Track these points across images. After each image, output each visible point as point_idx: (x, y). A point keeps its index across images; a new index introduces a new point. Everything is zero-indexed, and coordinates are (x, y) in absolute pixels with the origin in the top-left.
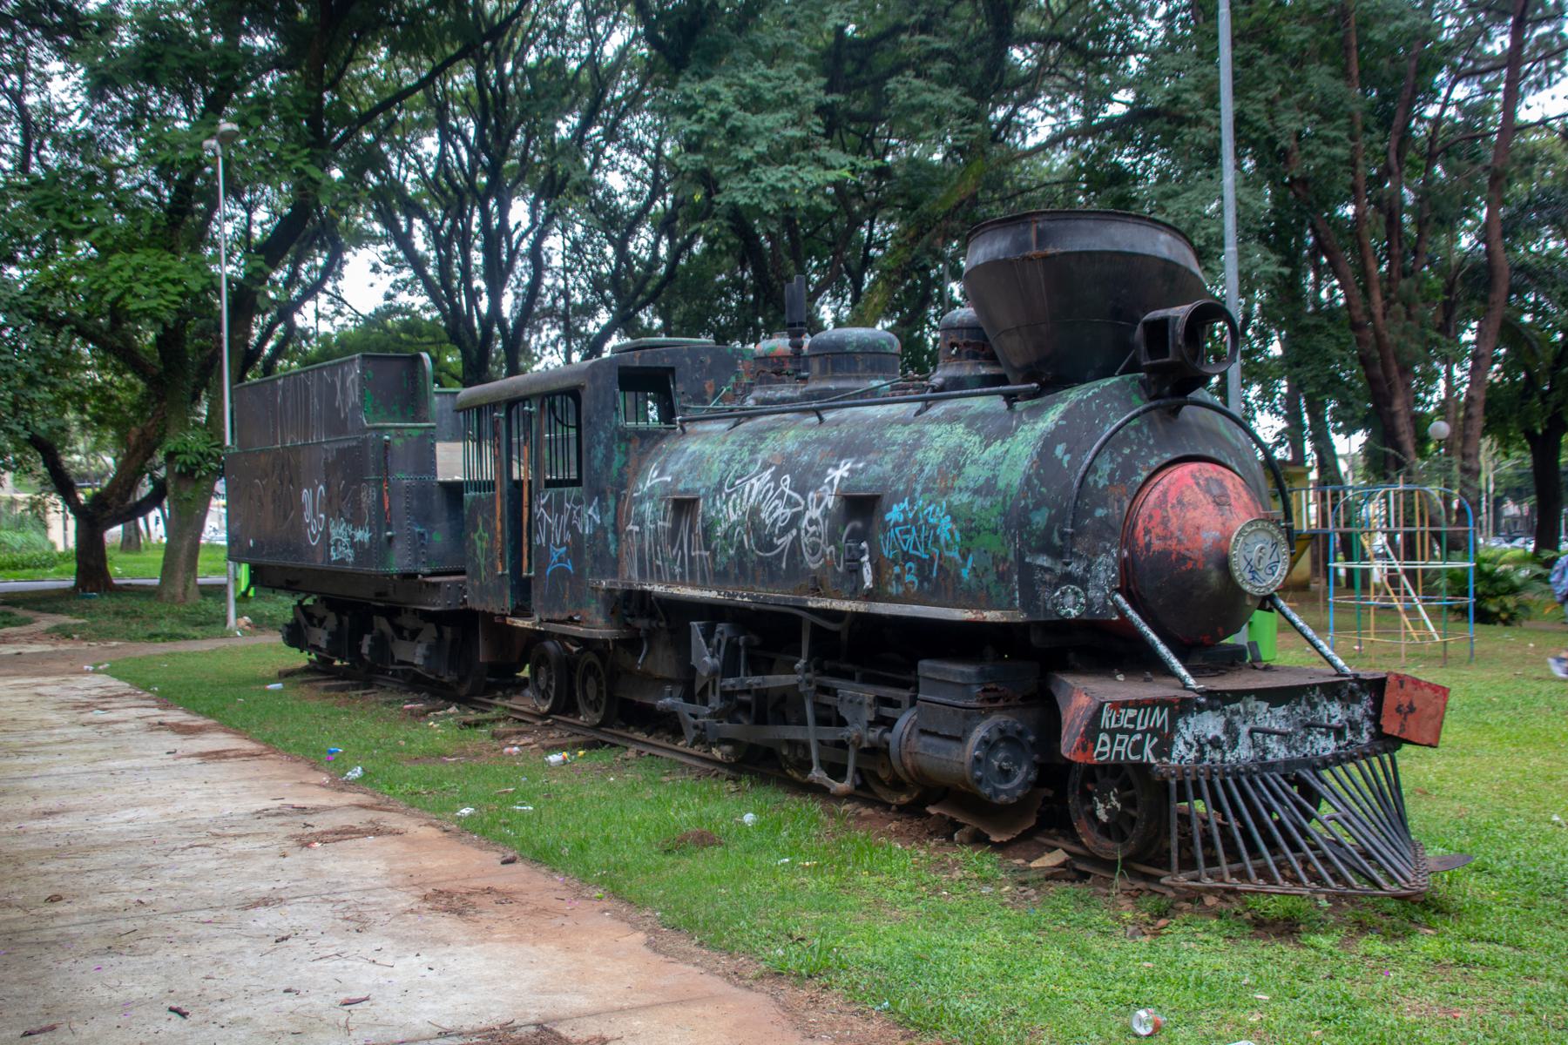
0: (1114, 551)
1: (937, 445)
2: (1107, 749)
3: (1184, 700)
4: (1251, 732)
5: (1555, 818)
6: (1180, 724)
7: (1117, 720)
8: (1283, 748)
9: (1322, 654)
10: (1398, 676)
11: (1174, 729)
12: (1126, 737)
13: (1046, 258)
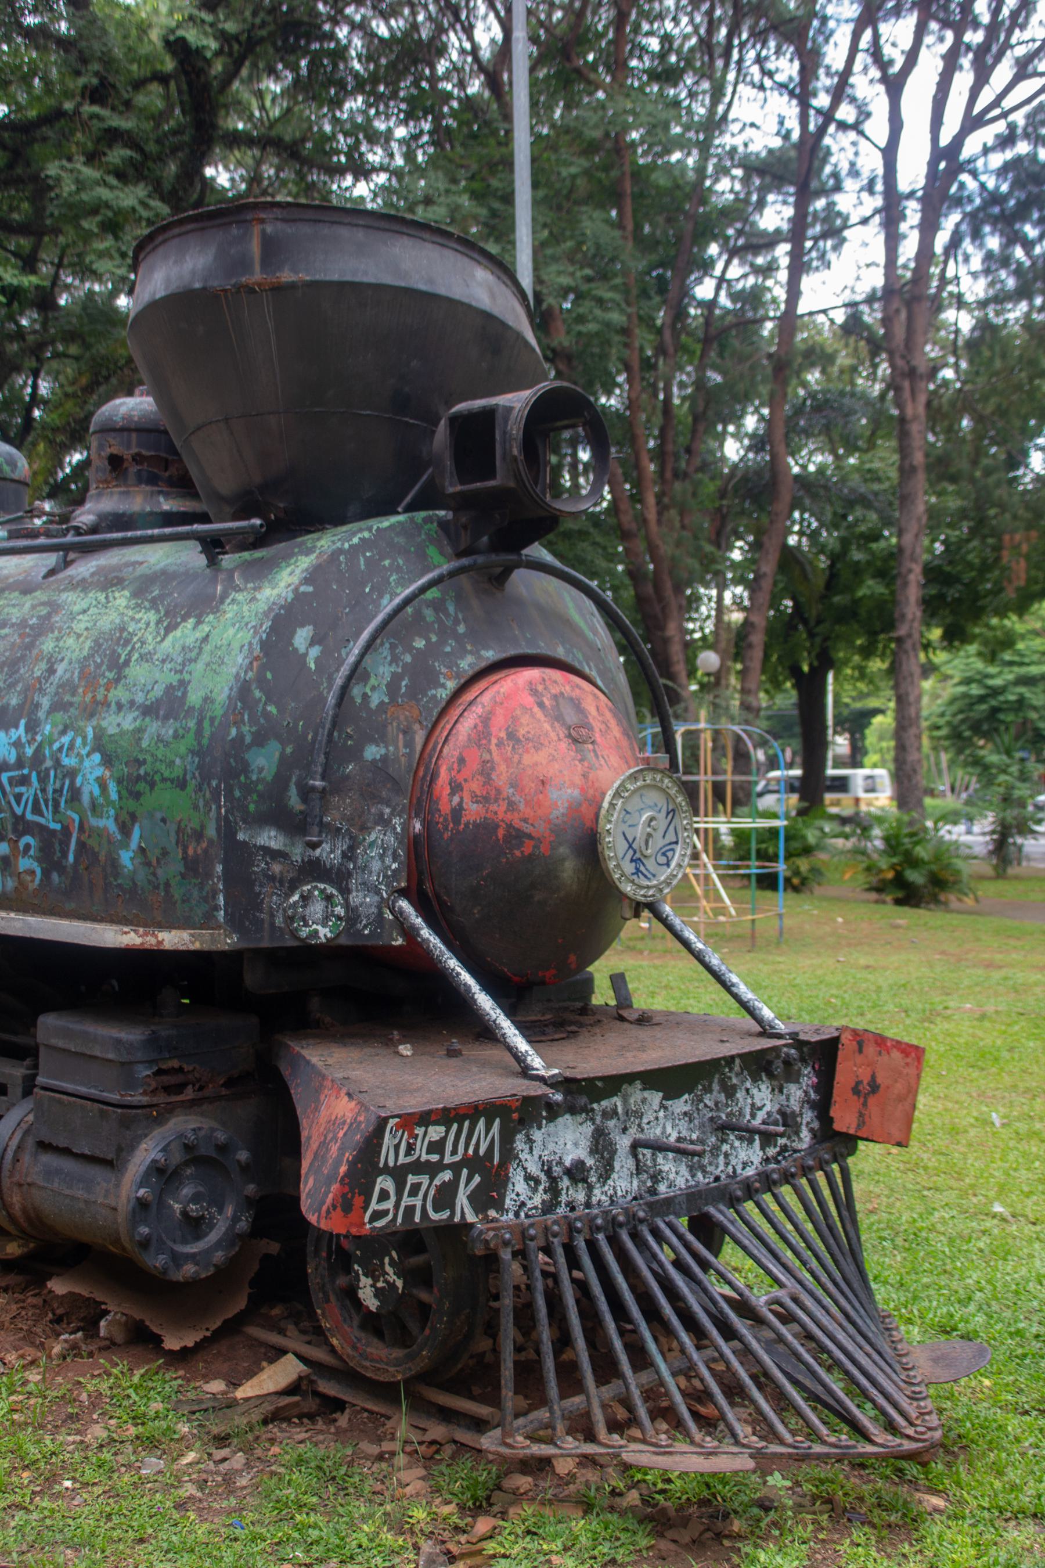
0: (396, 821)
1: (79, 626)
2: (389, 1205)
3: (528, 1100)
4: (635, 1146)
5: (998, 1208)
6: (520, 1143)
7: (410, 1148)
8: (684, 1170)
9: (736, 997)
10: (855, 1032)
11: (509, 1154)
12: (425, 1180)
13: (279, 289)
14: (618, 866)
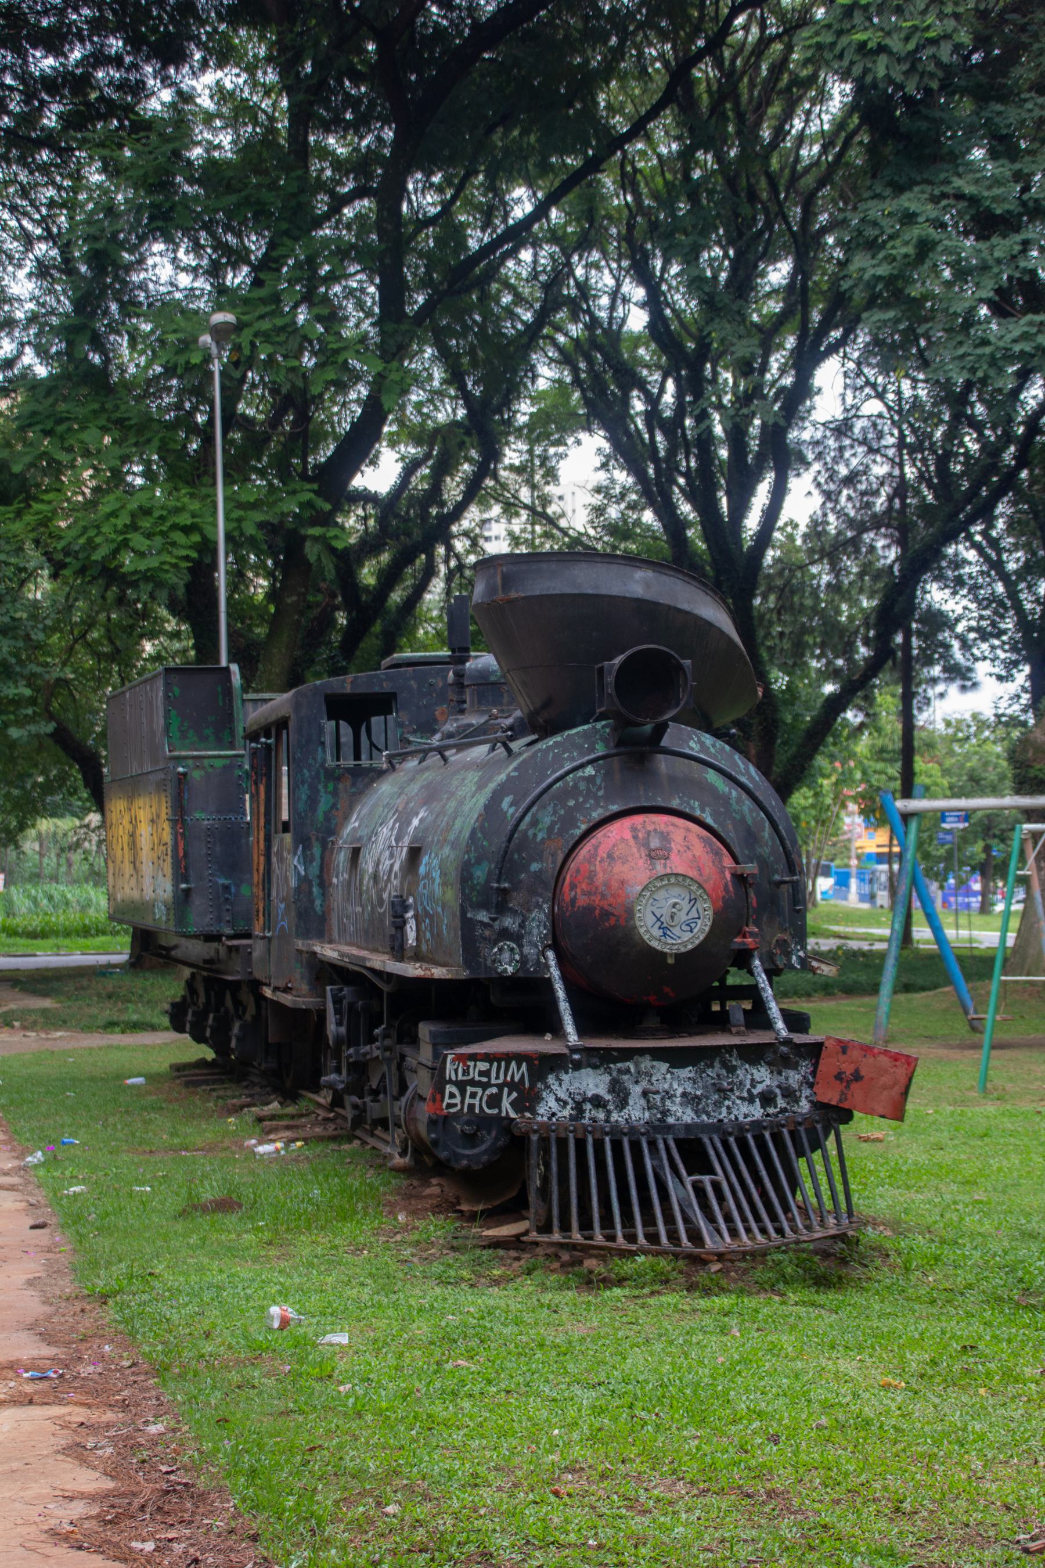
2: (457, 1100)
8: (689, 1111)
10: (839, 1041)
12: (479, 1091)
13: (511, 602)
14: (647, 931)
